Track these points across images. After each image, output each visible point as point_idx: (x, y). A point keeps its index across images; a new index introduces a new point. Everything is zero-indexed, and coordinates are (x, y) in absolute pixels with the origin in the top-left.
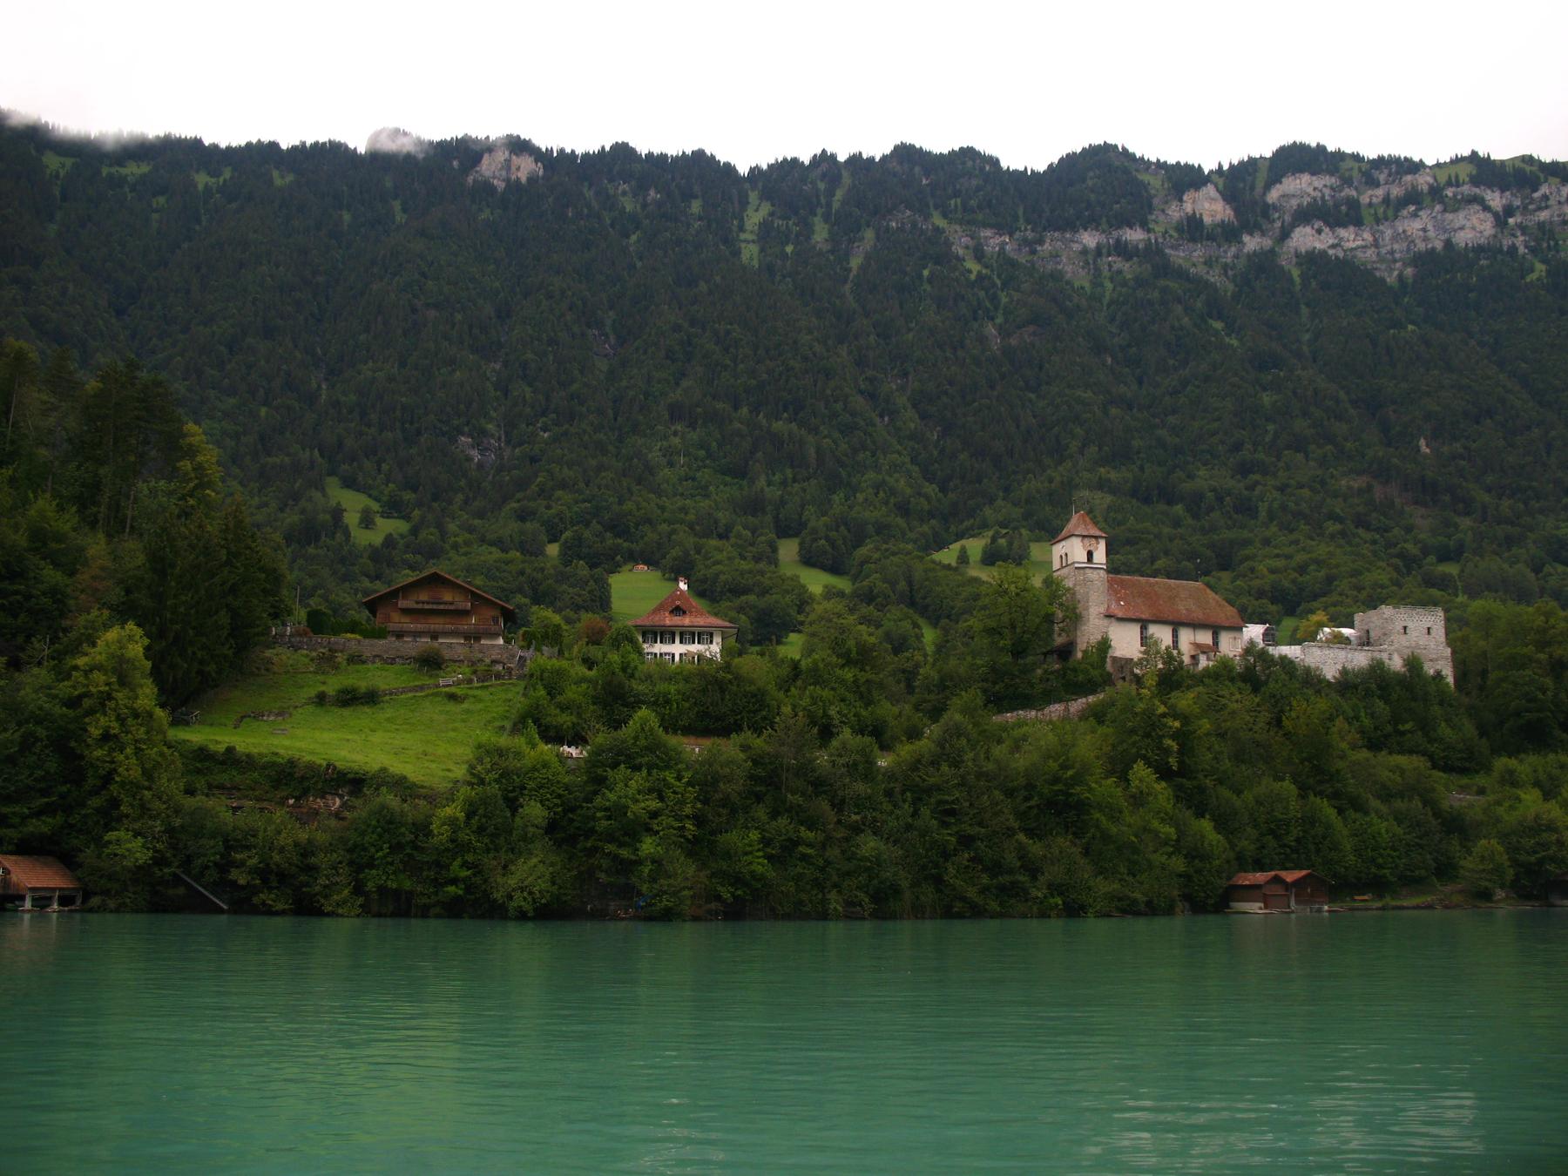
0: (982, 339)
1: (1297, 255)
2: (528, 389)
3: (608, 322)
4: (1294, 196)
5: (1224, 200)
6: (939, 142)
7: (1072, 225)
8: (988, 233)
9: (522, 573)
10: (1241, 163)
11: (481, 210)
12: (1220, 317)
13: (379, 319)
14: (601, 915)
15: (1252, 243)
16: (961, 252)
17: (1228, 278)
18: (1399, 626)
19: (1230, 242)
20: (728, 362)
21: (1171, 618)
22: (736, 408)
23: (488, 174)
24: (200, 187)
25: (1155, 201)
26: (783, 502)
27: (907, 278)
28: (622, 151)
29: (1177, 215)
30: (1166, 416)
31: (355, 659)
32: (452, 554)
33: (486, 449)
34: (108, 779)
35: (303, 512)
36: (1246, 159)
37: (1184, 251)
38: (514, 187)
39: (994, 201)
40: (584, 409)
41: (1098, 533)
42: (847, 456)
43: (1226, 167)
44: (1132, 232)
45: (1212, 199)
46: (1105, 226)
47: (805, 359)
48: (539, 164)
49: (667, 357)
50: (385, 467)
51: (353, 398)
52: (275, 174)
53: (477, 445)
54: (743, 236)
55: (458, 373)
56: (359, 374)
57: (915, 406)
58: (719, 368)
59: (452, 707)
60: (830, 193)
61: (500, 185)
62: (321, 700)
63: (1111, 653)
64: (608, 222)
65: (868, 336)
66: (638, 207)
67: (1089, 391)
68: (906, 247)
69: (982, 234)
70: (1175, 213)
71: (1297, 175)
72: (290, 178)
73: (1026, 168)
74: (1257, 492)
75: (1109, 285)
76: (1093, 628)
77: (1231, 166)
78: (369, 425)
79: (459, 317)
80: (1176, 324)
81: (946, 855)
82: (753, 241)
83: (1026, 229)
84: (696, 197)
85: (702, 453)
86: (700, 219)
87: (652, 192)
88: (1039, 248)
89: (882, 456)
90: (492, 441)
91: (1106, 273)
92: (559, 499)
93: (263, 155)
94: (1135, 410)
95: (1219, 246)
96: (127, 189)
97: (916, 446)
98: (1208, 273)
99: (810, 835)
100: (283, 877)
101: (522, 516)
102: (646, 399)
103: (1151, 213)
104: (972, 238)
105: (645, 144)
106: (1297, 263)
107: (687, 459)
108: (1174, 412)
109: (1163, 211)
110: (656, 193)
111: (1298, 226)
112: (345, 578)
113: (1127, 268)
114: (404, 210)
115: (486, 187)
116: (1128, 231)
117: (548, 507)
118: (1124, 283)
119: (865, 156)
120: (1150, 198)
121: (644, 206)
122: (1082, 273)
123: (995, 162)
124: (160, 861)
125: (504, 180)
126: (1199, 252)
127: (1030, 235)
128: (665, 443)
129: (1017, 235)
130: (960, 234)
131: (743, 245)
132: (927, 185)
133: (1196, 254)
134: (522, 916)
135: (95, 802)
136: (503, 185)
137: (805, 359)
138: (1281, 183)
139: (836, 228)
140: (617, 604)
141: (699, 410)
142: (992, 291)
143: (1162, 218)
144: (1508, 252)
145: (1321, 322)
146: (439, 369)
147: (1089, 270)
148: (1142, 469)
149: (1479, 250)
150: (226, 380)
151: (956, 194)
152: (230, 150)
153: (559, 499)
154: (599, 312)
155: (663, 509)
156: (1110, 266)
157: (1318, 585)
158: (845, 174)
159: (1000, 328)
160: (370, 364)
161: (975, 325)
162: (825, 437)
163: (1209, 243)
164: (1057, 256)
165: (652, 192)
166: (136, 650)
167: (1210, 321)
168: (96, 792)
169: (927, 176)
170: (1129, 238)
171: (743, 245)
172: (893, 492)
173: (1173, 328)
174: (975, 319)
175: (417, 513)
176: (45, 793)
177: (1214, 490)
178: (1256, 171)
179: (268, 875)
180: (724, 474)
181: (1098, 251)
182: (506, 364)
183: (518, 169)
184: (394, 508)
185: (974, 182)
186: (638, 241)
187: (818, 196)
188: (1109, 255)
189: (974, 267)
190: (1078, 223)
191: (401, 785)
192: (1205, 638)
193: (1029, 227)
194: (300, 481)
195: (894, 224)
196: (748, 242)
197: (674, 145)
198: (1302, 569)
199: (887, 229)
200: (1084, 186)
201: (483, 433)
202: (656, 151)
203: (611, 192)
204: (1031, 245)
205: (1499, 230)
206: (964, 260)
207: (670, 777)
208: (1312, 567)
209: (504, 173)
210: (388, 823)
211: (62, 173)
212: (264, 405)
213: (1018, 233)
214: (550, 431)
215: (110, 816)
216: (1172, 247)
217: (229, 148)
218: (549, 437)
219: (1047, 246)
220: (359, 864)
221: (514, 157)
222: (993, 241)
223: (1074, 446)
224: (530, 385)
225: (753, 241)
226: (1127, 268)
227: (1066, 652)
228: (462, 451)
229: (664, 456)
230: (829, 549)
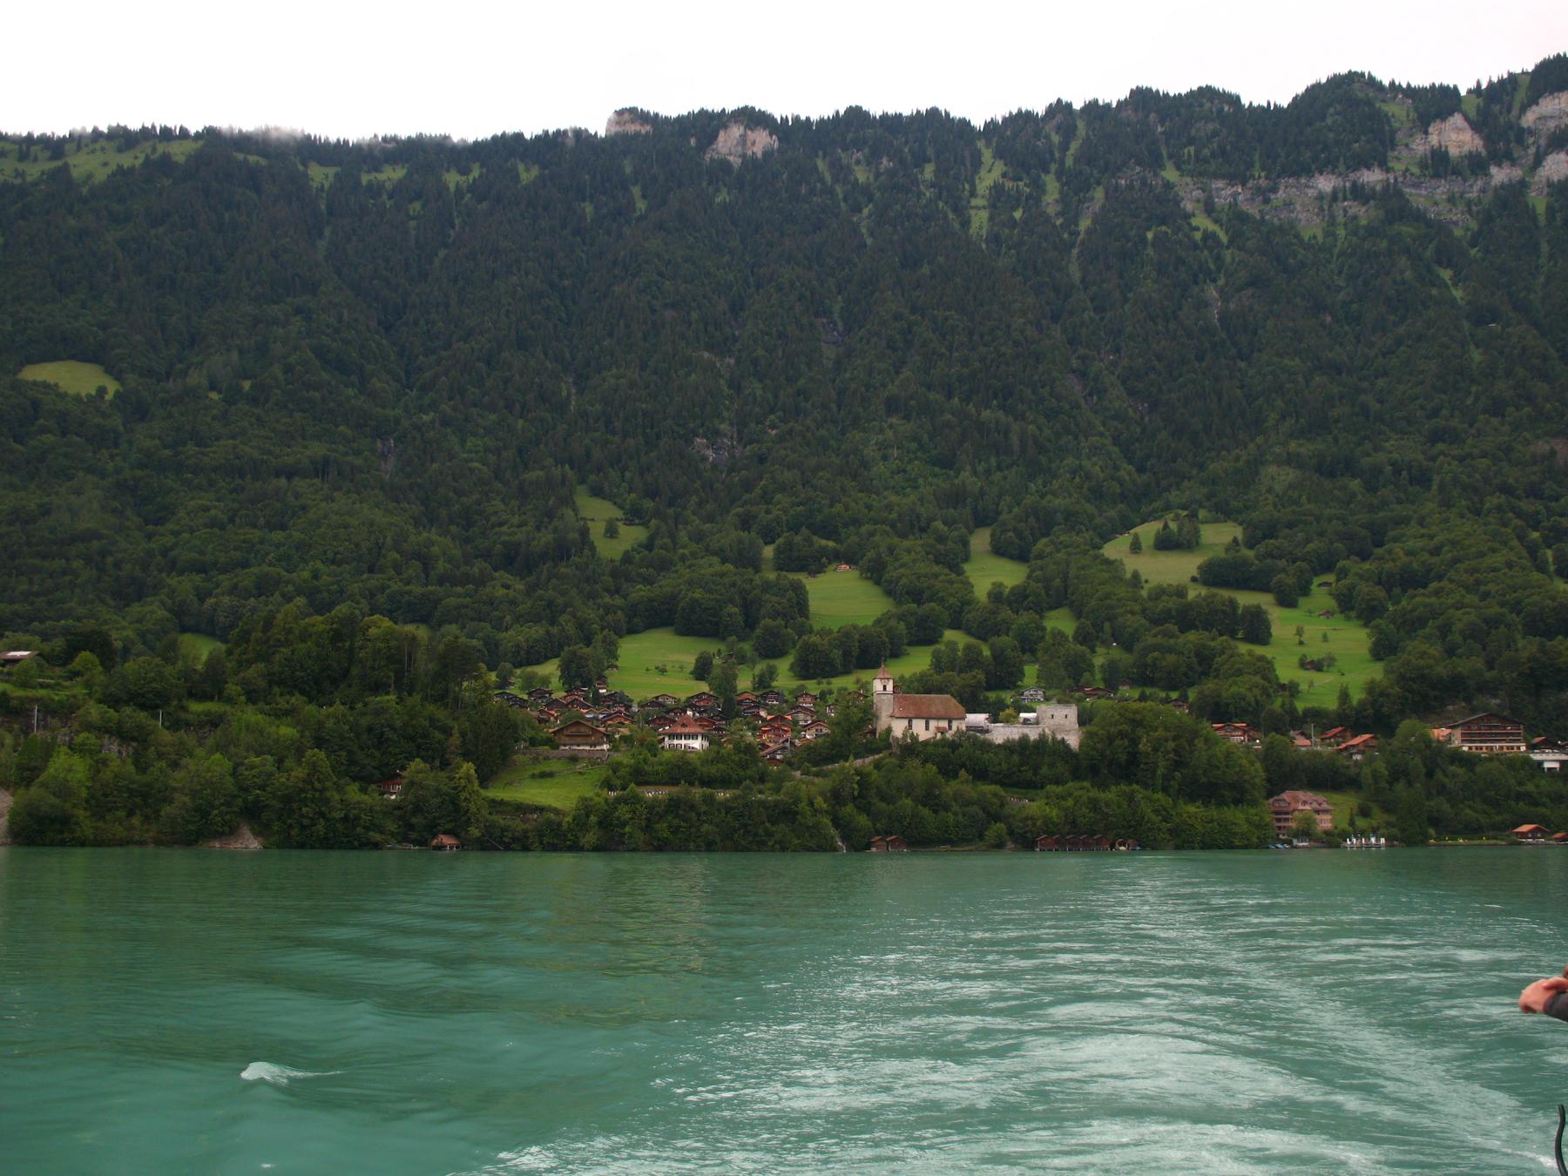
0: (1203, 304)
1: (1550, 184)
2: (759, 385)
3: (837, 308)
4: (1551, 117)
5: (1473, 129)
6: (1175, 83)
7: (1304, 170)
8: (1220, 184)
9: (734, 585)
10: (1501, 82)
11: (718, 190)
13: (622, 323)
14: (616, 850)
15: (1500, 175)
17: (1470, 215)
18: (1049, 715)
19: (1477, 175)
20: (943, 350)
22: (949, 397)
23: (724, 150)
24: (452, 187)
25: (1399, 135)
26: (982, 494)
27: (1130, 244)
28: (856, 115)
29: (1421, 148)
30: (1376, 378)
31: (546, 758)
32: (679, 566)
33: (720, 448)
34: (467, 812)
35: (555, 531)
36: (1505, 76)
37: (1426, 188)
38: (750, 163)
39: (1229, 147)
40: (809, 405)
42: (1050, 441)
43: (1484, 86)
44: (1370, 173)
45: (1460, 129)
46: (1342, 168)
47: (1016, 344)
48: (774, 137)
49: (889, 347)
50: (628, 475)
51: (598, 407)
52: (521, 167)
53: (712, 445)
54: (974, 202)
55: (693, 376)
56: (604, 381)
57: (1124, 383)
58: (935, 357)
59: (580, 777)
60: (1064, 147)
61: (735, 161)
62: (533, 776)
63: (892, 734)
64: (841, 196)
65: (1084, 311)
66: (871, 178)
67: (1297, 359)
68: (1133, 207)
69: (1213, 186)
70: (1420, 146)
71: (1556, 94)
72: (535, 171)
73: (1269, 103)
74: (1438, 463)
75: (1341, 232)
76: (883, 722)
77: (1491, 84)
78: (614, 433)
79: (695, 315)
80: (1399, 278)
81: (736, 831)
82: (984, 207)
83: (1260, 177)
84: (929, 161)
85: (914, 445)
86: (933, 185)
87: (885, 160)
88: (1273, 197)
89: (1083, 439)
90: (725, 440)
91: (1341, 219)
92: (779, 503)
93: (508, 147)
94: (1344, 375)
95: (1465, 180)
96: (385, 197)
97: (1119, 426)
98: (1451, 210)
99: (685, 825)
100: (518, 839)
101: (745, 523)
102: (867, 391)
103: (1393, 149)
104: (1204, 191)
105: (877, 107)
106: (1548, 194)
107: (900, 451)
108: (1385, 374)
109: (1407, 145)
110: (889, 161)
111: (1551, 153)
112: (591, 596)
113: (1364, 213)
114: (644, 197)
115: (724, 166)
116: (1366, 172)
117: (768, 512)
119: (1101, 103)
120: (1393, 132)
121: (878, 175)
122: (1317, 220)
123: (1234, 100)
124: (483, 836)
125: (740, 156)
126: (1442, 189)
127: (1263, 183)
128: (880, 437)
129: (1250, 184)
130: (1191, 186)
131: (972, 212)
132: (1162, 133)
133: (1439, 191)
134: (588, 850)
135: (463, 818)
136: (740, 161)
137: (1016, 344)
138: (1537, 104)
139: (1065, 188)
140: (814, 605)
141: (913, 402)
142: (1216, 251)
143: (1405, 153)
145: (1556, 264)
146: (676, 371)
147: (1324, 217)
148: (1336, 440)
150: (486, 397)
151: (1191, 142)
152: (478, 146)
153: (779, 503)
154: (827, 301)
155: (869, 508)
156: (1345, 211)
157: (1443, 567)
158: (1081, 125)
159: (1221, 291)
160: (614, 371)
161: (1196, 289)
162: (1031, 423)
163: (1454, 177)
164: (1291, 204)
165: (885, 160)
166: (472, 772)
168: (463, 815)
169: (1162, 122)
170: (1366, 180)
171: (972, 212)
172: (1088, 477)
173: (1395, 282)
174: (1196, 283)
175: (653, 522)
176: (449, 816)
177: (1393, 464)
178: (1515, 89)
179: (514, 839)
180: (934, 464)
182: (738, 362)
183: (754, 143)
184: (635, 516)
185: (1211, 127)
186: (870, 215)
187: (1052, 154)
188: (1345, 199)
190: (1313, 167)
191: (556, 811)
192: (944, 724)
193: (1263, 174)
194: (553, 498)
195: (1123, 182)
196: (978, 208)
197: (906, 104)
198: (1436, 551)
199: (1117, 188)
200: (1324, 124)
201: (717, 433)
202: (891, 111)
203: (845, 161)
204: (1264, 195)
207: (638, 806)
208: (1446, 548)
209: (740, 149)
210: (549, 822)
211: (326, 186)
212: (521, 417)
213: (1251, 181)
214: (777, 428)
215: (468, 823)
216: (1414, 186)
217: (476, 143)
218: (776, 435)
219: (1281, 194)
220: (541, 835)
221: (749, 132)
222: (1224, 193)
223: (1273, 417)
224: (761, 381)
225: (984, 207)
226: (1364, 213)
227: (873, 732)
228: (698, 452)
229: (880, 450)
230: (1016, 541)
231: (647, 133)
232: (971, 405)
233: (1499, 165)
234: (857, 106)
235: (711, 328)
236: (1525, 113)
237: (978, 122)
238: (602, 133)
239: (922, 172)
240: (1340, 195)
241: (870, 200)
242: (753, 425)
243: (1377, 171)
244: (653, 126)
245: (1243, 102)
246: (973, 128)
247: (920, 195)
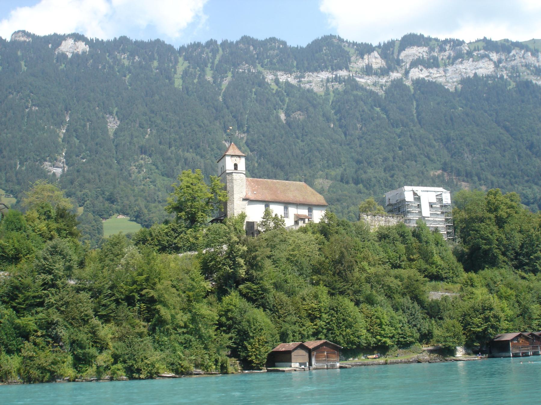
7: (316, 70)
12: (380, 106)
16: (269, 81)
21: (283, 201)
23: (64, 50)
38: (76, 56)
41: (241, 154)
43: (382, 45)
46: (330, 69)
60: (214, 57)
83: (297, 72)
111: (412, 68)
118: (339, 94)
119: (229, 42)
121: (133, 63)
138: (405, 50)
144: (500, 78)
149: (488, 77)
151: (268, 57)
156: (333, 86)
167: (375, 108)
171: (176, 80)
181: (328, 80)
189: (274, 87)
192: (304, 212)
203: (118, 58)
205: (496, 68)
206: (271, 85)
216: (360, 78)
226: (340, 87)
231: (29, 41)
232: (180, 151)
233: (393, 72)
234: (124, 36)
235: (55, 116)
236: (400, 54)
237: (177, 47)
238: (8, 39)
239: (153, 64)
240: (330, 80)
241: (130, 73)
242: (74, 157)
243: (345, 71)
244: (32, 38)
245: (288, 45)
246: (174, 49)
247: (152, 71)
